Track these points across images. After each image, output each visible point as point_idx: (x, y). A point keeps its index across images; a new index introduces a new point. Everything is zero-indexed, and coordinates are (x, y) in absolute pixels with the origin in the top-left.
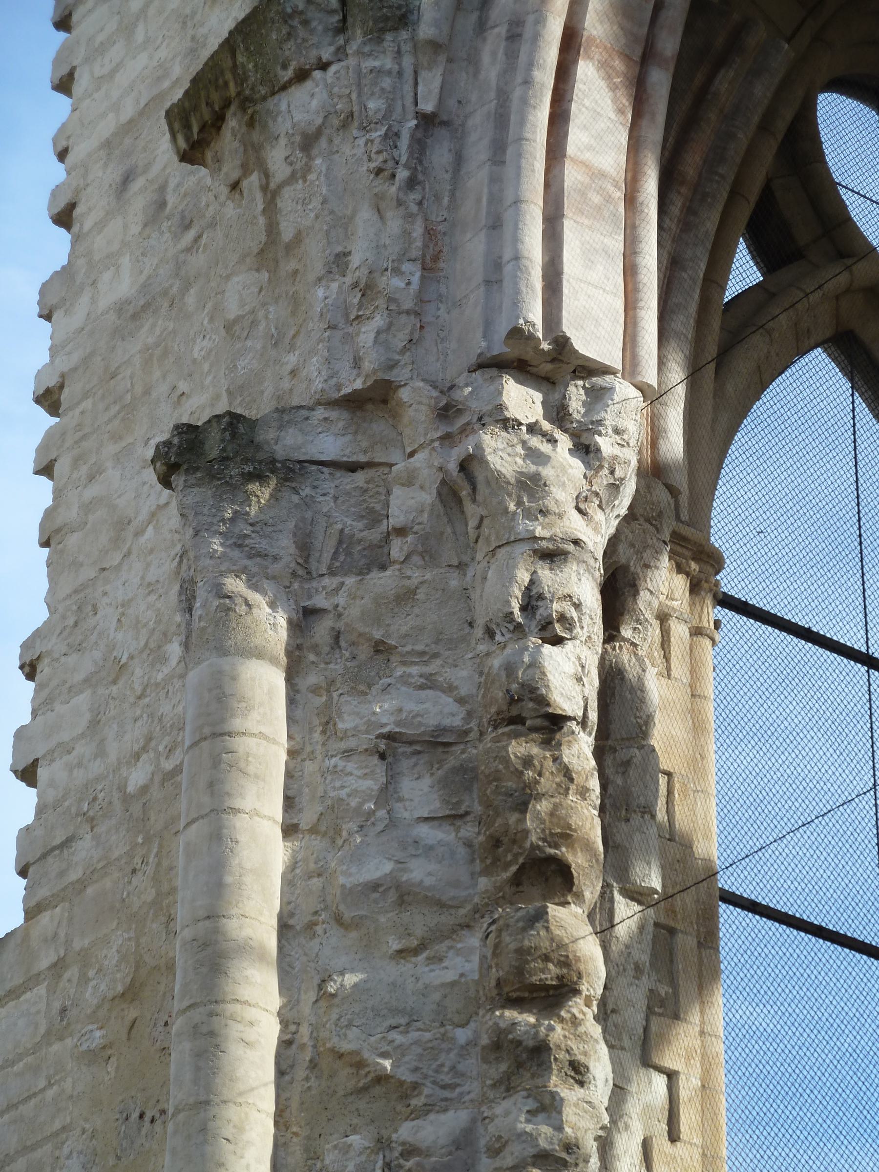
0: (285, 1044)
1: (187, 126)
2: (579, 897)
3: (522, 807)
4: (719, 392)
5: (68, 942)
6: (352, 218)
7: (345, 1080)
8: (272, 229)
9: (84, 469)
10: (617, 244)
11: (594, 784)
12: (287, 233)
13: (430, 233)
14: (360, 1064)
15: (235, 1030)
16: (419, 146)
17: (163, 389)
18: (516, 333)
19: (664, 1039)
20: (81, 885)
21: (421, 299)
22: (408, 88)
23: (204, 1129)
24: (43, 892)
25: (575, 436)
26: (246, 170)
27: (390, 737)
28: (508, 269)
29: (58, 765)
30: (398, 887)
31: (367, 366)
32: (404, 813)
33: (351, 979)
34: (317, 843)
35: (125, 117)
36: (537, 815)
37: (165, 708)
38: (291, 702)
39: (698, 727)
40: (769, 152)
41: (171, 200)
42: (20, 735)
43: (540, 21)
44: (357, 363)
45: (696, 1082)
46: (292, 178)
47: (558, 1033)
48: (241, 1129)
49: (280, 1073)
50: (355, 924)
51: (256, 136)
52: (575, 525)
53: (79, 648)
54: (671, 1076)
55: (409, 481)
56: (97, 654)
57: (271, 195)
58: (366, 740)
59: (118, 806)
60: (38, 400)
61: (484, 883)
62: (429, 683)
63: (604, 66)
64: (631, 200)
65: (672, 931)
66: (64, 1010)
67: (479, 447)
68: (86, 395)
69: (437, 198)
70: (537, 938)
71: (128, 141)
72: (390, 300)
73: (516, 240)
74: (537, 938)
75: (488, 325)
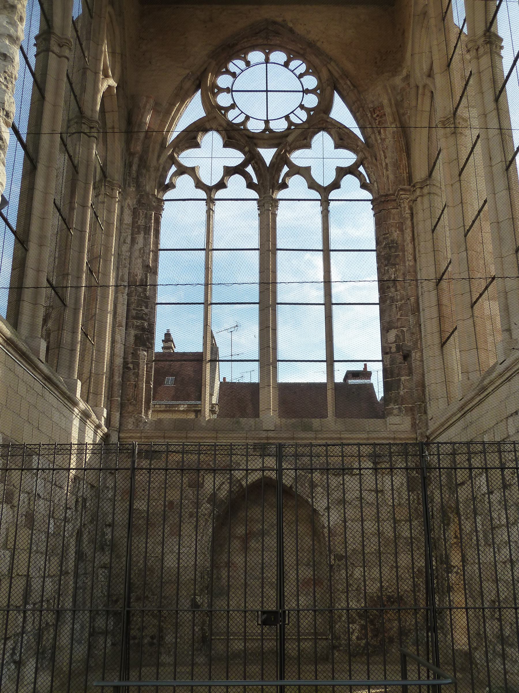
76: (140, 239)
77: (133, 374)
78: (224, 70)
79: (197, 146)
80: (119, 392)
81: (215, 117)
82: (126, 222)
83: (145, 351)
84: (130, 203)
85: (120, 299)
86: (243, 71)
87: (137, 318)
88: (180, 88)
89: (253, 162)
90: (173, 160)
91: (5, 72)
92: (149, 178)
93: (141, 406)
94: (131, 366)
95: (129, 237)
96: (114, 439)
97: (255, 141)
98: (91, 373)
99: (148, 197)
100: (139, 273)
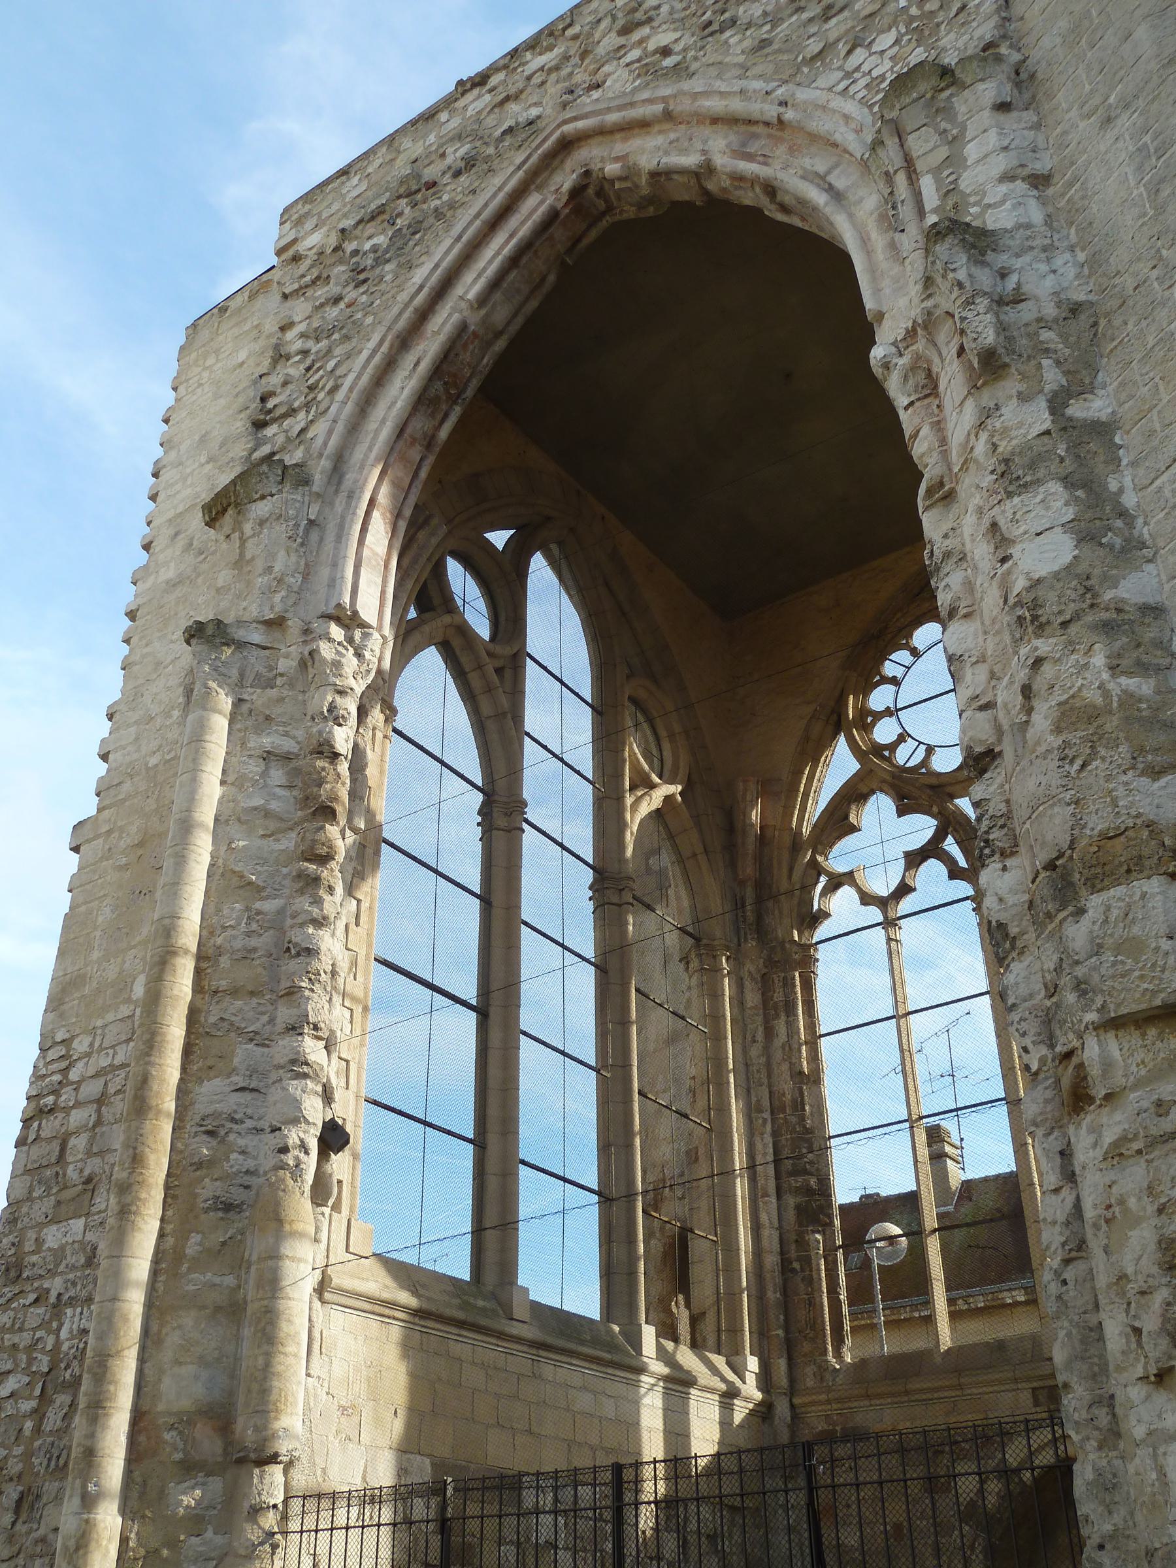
0: (212, 865)
1: (211, 512)
2: (338, 823)
3: (320, 786)
4: (402, 651)
5: (115, 822)
6: (276, 554)
7: (235, 881)
8: (242, 554)
9: (144, 642)
10: (379, 581)
11: (348, 781)
12: (248, 556)
13: (307, 565)
14: (242, 877)
15: (193, 856)
16: (307, 532)
17: (183, 614)
18: (339, 605)
19: (358, 887)
20: (124, 800)
21: (300, 588)
22: (306, 509)
23: (175, 894)
24: (107, 802)
25: (355, 649)
26: (234, 531)
27: (268, 752)
28: (338, 581)
29: (119, 753)
30: (265, 810)
31: (277, 609)
32: (270, 782)
33: (242, 843)
34: (233, 789)
35: (178, 511)
36: (325, 790)
37: (169, 735)
38: (229, 733)
39: (382, 772)
40: (429, 567)
41: (195, 543)
42: (102, 741)
43: (362, 491)
44: (272, 608)
45: (367, 905)
46: (254, 535)
47: (325, 874)
48: (191, 896)
49: (209, 876)
50: (246, 822)
51: (240, 518)
52: (351, 682)
53: (134, 709)
54: (359, 901)
55: (287, 656)
56: (141, 712)
57: (243, 541)
58: (259, 752)
59: (144, 771)
60: (126, 615)
61: (300, 813)
62: (286, 734)
63: (383, 514)
64: (386, 567)
65: (365, 846)
66: (110, 849)
67: (318, 647)
68: (148, 614)
69: (311, 552)
70: (320, 836)
71: (179, 520)
72: (289, 586)
73: (343, 571)
74: (320, 836)
75: (327, 601)
76: (781, 1027)
77: (803, 1280)
78: (878, 678)
79: (854, 829)
80: (778, 1319)
81: (871, 771)
82: (749, 1004)
83: (818, 1232)
84: (752, 969)
85: (759, 1146)
86: (909, 668)
87: (795, 1173)
88: (806, 738)
89: (950, 830)
90: (818, 870)
91: (308, 972)
92: (781, 913)
93: (825, 1343)
94: (796, 1265)
95: (761, 1030)
96: (782, 1408)
97: (949, 789)
98: (718, 1293)
99: (783, 948)
100: (786, 1086)
